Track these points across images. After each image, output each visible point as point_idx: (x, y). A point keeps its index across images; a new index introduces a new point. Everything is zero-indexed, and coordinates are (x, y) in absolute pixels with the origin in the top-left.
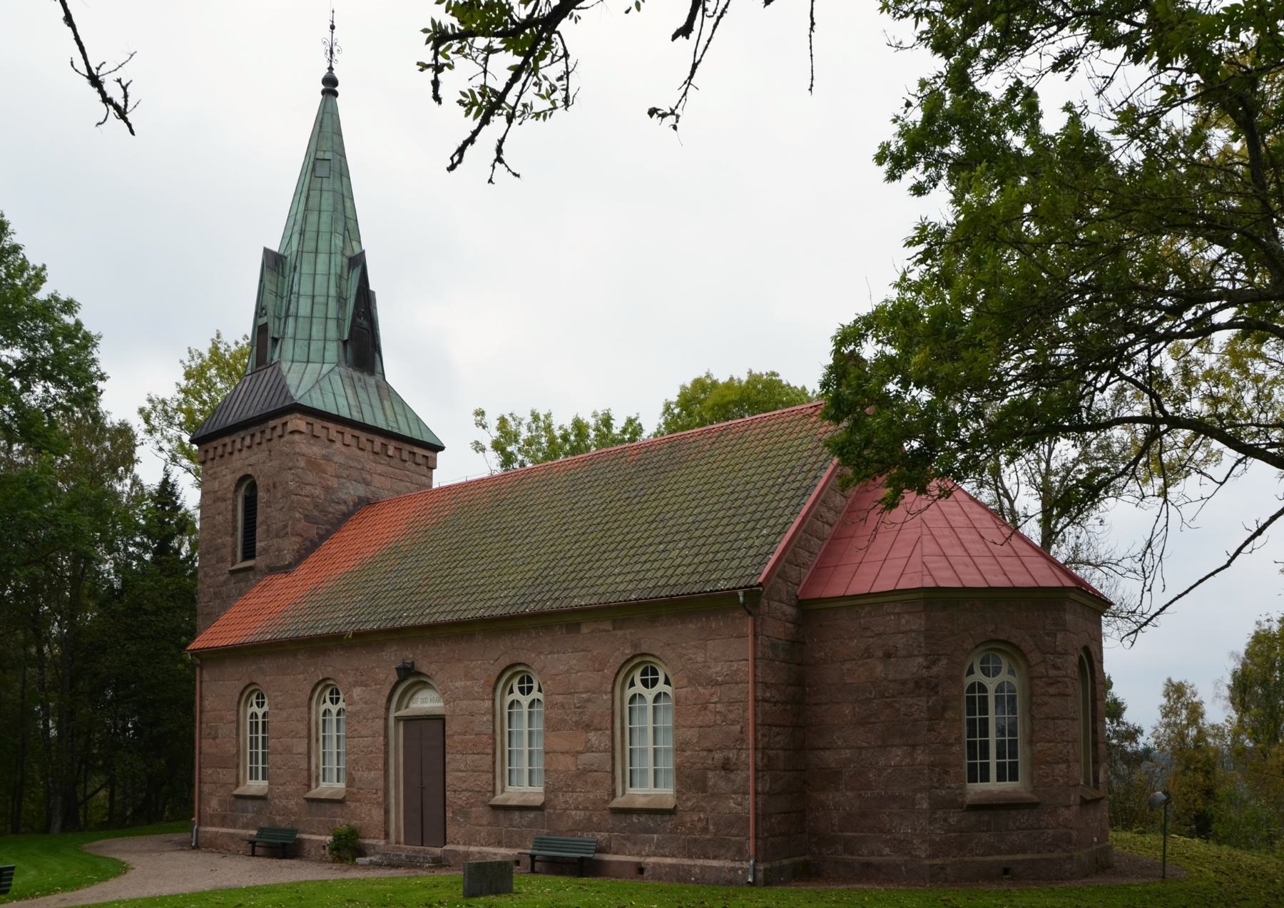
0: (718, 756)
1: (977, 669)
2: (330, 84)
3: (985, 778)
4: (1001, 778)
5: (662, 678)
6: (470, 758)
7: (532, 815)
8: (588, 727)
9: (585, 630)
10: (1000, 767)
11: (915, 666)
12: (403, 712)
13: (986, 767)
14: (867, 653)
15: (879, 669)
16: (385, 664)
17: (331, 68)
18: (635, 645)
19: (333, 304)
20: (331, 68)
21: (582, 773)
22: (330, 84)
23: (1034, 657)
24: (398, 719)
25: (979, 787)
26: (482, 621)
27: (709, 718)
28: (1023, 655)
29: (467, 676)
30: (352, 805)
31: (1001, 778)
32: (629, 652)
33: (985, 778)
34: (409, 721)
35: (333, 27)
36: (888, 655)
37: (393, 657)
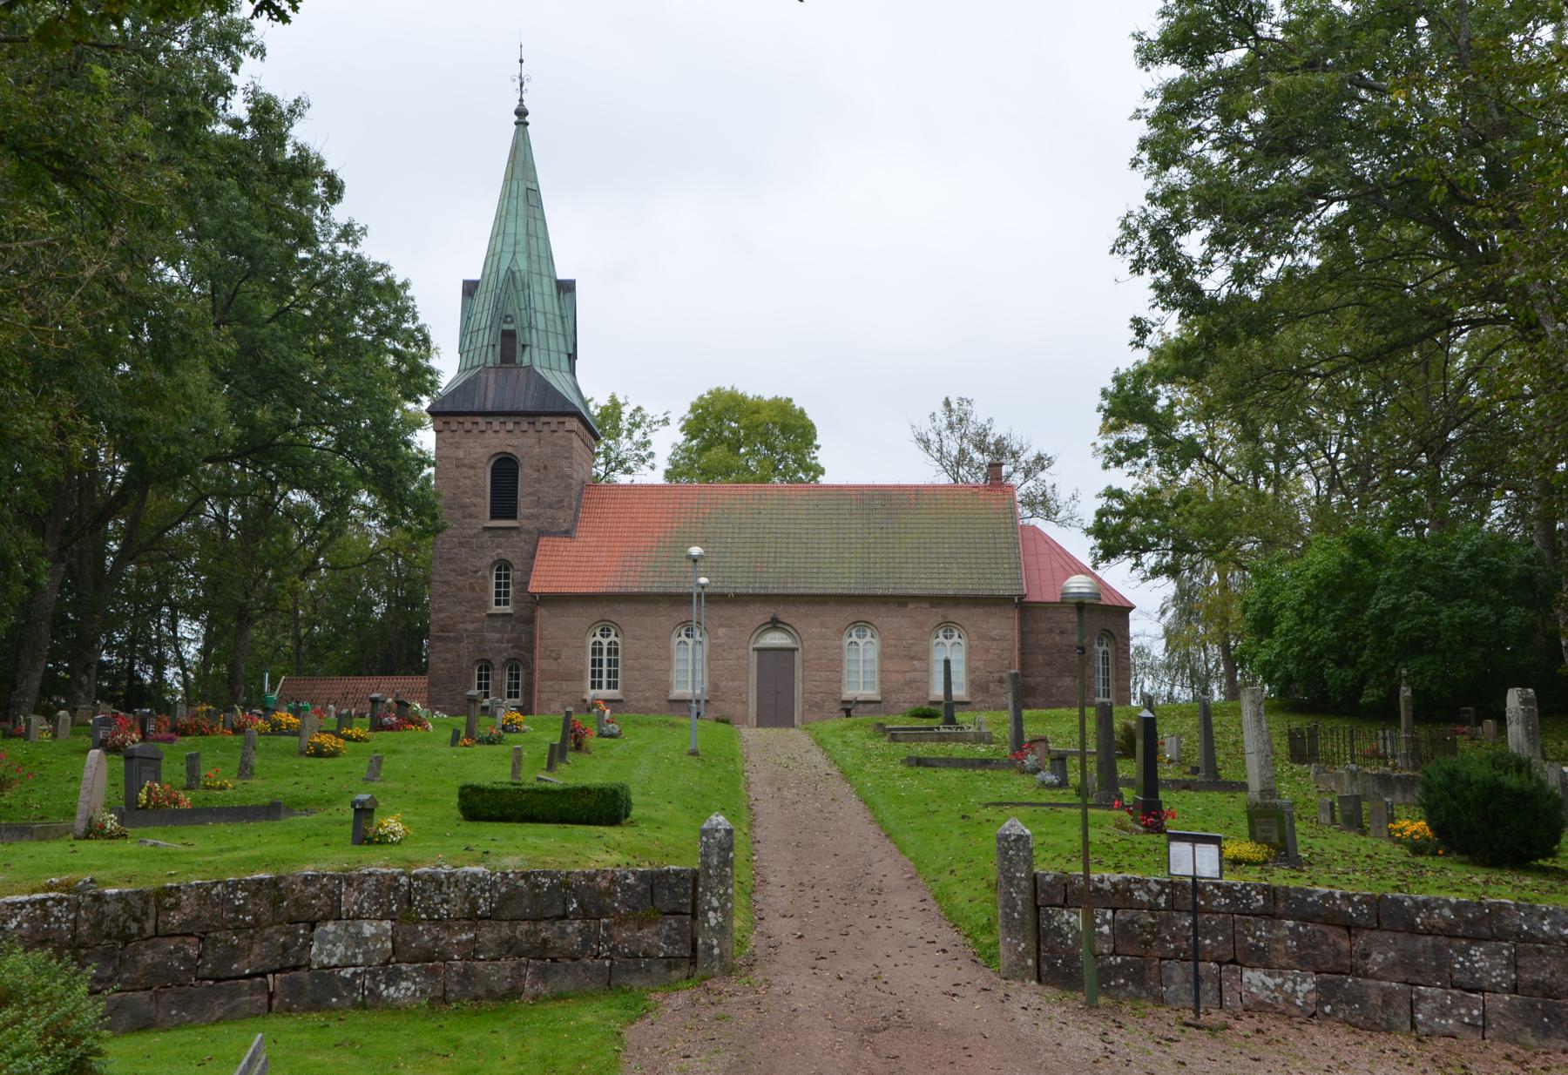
0: (996, 675)
1: (598, 634)
2: (521, 113)
3: (600, 687)
4: (609, 687)
5: (613, 633)
6: (823, 674)
7: (872, 706)
8: (913, 658)
9: (911, 606)
10: (609, 683)
11: (1075, 639)
12: (757, 646)
13: (600, 683)
14: (1051, 631)
15: (1058, 639)
16: (761, 614)
17: (521, 100)
18: (944, 617)
19: (559, 322)
20: (521, 100)
21: (908, 683)
22: (521, 113)
23: (1118, 639)
24: (754, 649)
25: (597, 691)
26: (802, 595)
27: (991, 656)
28: (1114, 638)
29: (822, 625)
30: (717, 704)
31: (609, 687)
32: (940, 620)
33: (600, 687)
34: (759, 650)
35: (521, 61)
36: (1062, 632)
37: (770, 611)
